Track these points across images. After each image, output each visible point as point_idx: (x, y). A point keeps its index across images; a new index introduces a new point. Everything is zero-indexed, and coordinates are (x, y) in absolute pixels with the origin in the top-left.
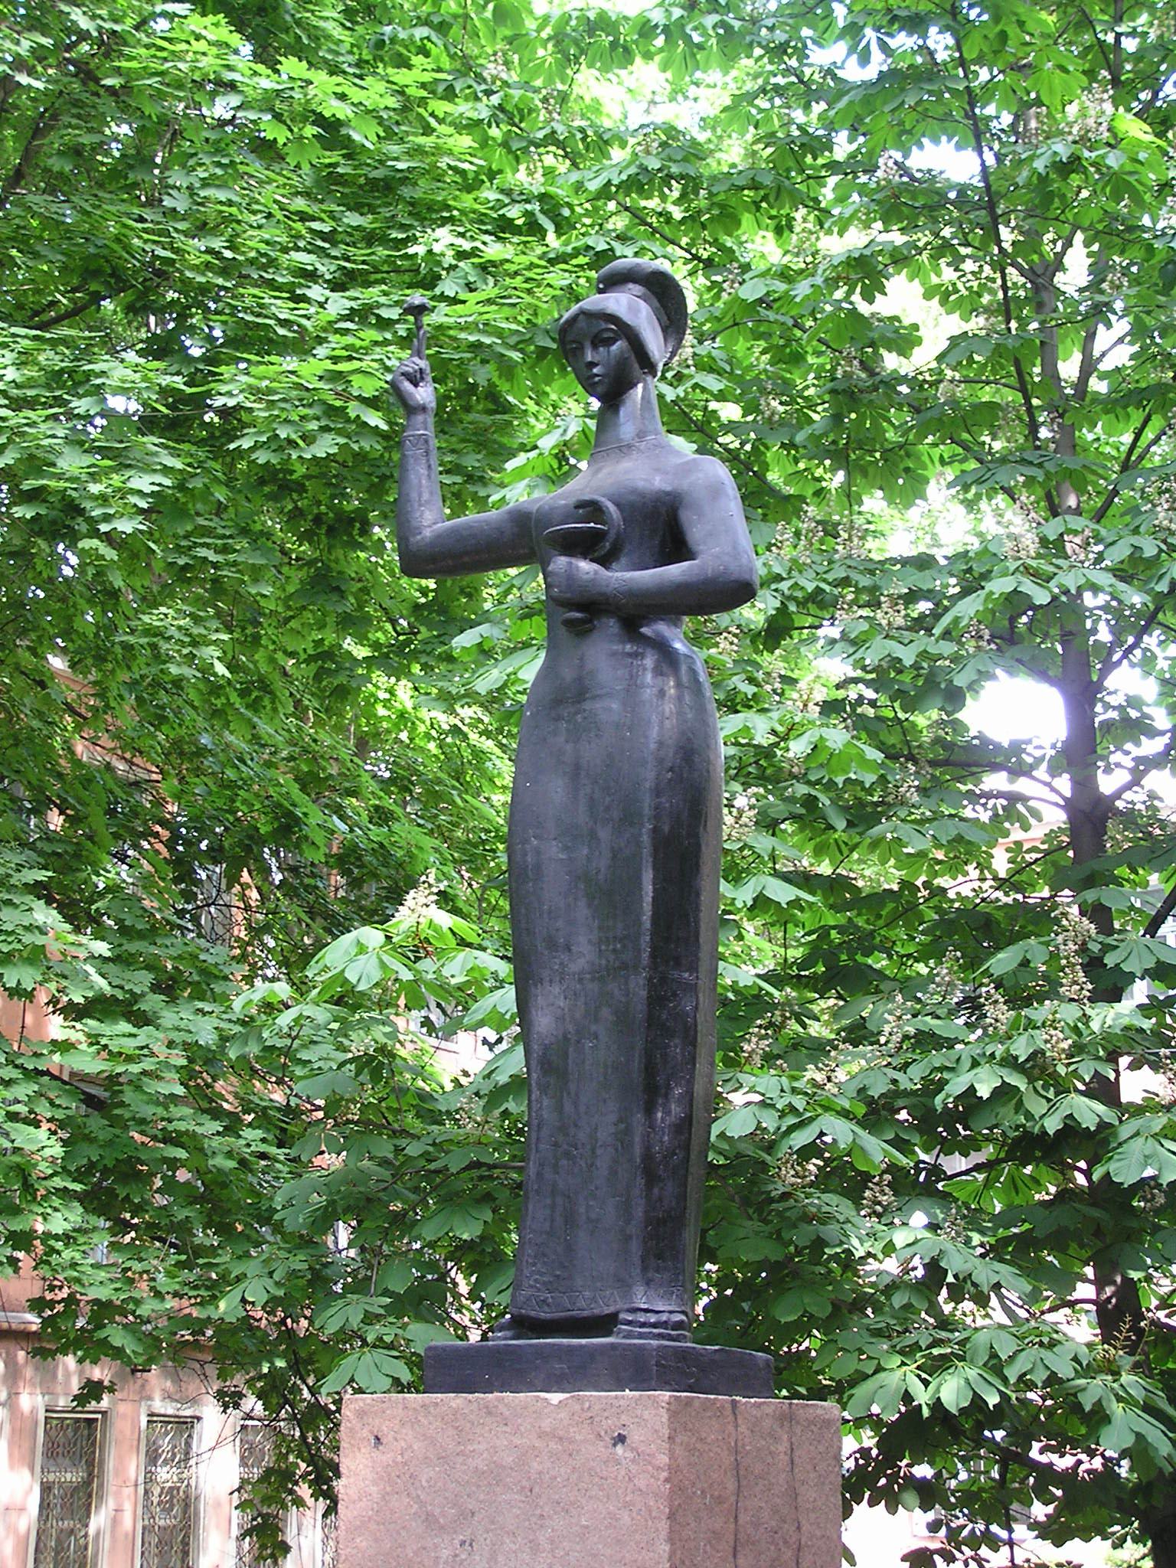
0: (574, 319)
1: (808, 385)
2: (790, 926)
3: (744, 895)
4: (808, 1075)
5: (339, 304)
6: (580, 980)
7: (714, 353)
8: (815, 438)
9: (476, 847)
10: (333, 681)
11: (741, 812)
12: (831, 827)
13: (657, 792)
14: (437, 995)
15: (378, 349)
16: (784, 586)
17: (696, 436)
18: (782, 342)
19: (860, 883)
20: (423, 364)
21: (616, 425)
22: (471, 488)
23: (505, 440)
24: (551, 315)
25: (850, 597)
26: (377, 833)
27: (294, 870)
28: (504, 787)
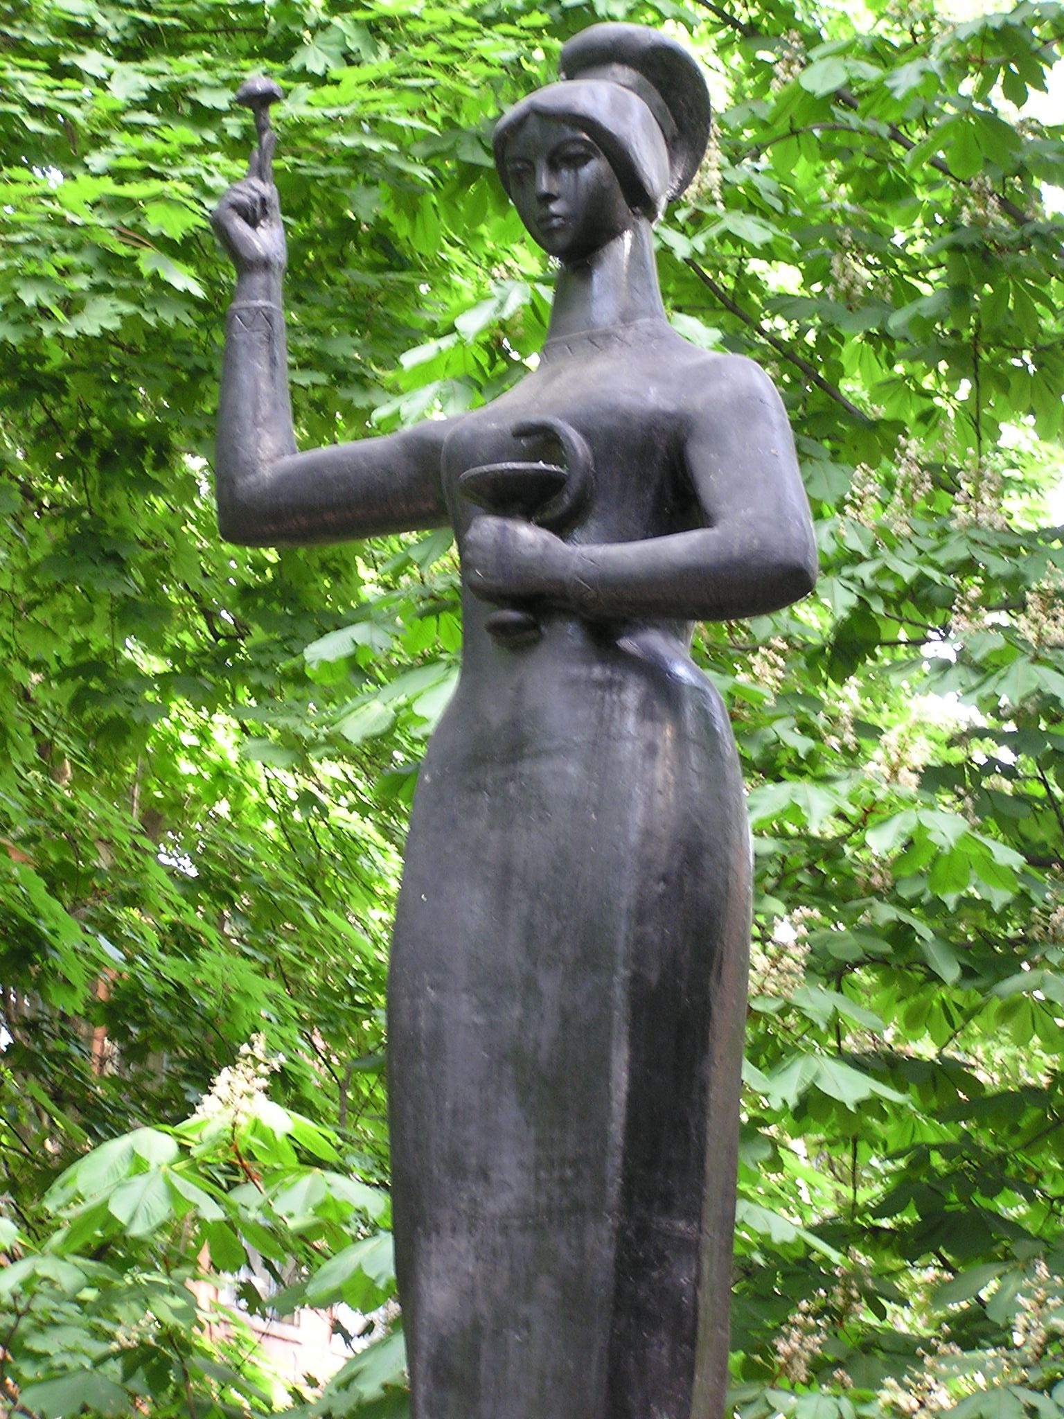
0: (519, 124)
1: (910, 235)
2: (863, 1147)
3: (783, 1089)
4: (885, 1396)
5: (130, 81)
6: (504, 1230)
7: (759, 181)
8: (922, 324)
9: (338, 997)
10: (106, 718)
11: (782, 950)
12: (934, 978)
13: (640, 915)
14: (264, 1246)
15: (192, 158)
16: (865, 571)
17: (724, 317)
18: (870, 164)
19: (981, 1076)
20: (268, 190)
21: (587, 300)
22: (343, 394)
23: (402, 316)
24: (487, 111)
25: (974, 593)
26: (174, 969)
27: (32, 1026)
28: (387, 898)
